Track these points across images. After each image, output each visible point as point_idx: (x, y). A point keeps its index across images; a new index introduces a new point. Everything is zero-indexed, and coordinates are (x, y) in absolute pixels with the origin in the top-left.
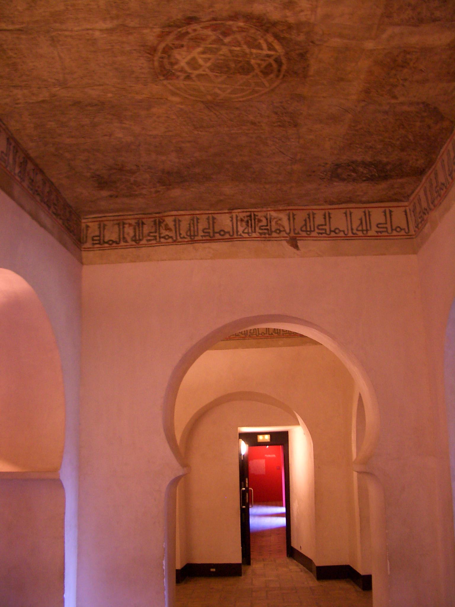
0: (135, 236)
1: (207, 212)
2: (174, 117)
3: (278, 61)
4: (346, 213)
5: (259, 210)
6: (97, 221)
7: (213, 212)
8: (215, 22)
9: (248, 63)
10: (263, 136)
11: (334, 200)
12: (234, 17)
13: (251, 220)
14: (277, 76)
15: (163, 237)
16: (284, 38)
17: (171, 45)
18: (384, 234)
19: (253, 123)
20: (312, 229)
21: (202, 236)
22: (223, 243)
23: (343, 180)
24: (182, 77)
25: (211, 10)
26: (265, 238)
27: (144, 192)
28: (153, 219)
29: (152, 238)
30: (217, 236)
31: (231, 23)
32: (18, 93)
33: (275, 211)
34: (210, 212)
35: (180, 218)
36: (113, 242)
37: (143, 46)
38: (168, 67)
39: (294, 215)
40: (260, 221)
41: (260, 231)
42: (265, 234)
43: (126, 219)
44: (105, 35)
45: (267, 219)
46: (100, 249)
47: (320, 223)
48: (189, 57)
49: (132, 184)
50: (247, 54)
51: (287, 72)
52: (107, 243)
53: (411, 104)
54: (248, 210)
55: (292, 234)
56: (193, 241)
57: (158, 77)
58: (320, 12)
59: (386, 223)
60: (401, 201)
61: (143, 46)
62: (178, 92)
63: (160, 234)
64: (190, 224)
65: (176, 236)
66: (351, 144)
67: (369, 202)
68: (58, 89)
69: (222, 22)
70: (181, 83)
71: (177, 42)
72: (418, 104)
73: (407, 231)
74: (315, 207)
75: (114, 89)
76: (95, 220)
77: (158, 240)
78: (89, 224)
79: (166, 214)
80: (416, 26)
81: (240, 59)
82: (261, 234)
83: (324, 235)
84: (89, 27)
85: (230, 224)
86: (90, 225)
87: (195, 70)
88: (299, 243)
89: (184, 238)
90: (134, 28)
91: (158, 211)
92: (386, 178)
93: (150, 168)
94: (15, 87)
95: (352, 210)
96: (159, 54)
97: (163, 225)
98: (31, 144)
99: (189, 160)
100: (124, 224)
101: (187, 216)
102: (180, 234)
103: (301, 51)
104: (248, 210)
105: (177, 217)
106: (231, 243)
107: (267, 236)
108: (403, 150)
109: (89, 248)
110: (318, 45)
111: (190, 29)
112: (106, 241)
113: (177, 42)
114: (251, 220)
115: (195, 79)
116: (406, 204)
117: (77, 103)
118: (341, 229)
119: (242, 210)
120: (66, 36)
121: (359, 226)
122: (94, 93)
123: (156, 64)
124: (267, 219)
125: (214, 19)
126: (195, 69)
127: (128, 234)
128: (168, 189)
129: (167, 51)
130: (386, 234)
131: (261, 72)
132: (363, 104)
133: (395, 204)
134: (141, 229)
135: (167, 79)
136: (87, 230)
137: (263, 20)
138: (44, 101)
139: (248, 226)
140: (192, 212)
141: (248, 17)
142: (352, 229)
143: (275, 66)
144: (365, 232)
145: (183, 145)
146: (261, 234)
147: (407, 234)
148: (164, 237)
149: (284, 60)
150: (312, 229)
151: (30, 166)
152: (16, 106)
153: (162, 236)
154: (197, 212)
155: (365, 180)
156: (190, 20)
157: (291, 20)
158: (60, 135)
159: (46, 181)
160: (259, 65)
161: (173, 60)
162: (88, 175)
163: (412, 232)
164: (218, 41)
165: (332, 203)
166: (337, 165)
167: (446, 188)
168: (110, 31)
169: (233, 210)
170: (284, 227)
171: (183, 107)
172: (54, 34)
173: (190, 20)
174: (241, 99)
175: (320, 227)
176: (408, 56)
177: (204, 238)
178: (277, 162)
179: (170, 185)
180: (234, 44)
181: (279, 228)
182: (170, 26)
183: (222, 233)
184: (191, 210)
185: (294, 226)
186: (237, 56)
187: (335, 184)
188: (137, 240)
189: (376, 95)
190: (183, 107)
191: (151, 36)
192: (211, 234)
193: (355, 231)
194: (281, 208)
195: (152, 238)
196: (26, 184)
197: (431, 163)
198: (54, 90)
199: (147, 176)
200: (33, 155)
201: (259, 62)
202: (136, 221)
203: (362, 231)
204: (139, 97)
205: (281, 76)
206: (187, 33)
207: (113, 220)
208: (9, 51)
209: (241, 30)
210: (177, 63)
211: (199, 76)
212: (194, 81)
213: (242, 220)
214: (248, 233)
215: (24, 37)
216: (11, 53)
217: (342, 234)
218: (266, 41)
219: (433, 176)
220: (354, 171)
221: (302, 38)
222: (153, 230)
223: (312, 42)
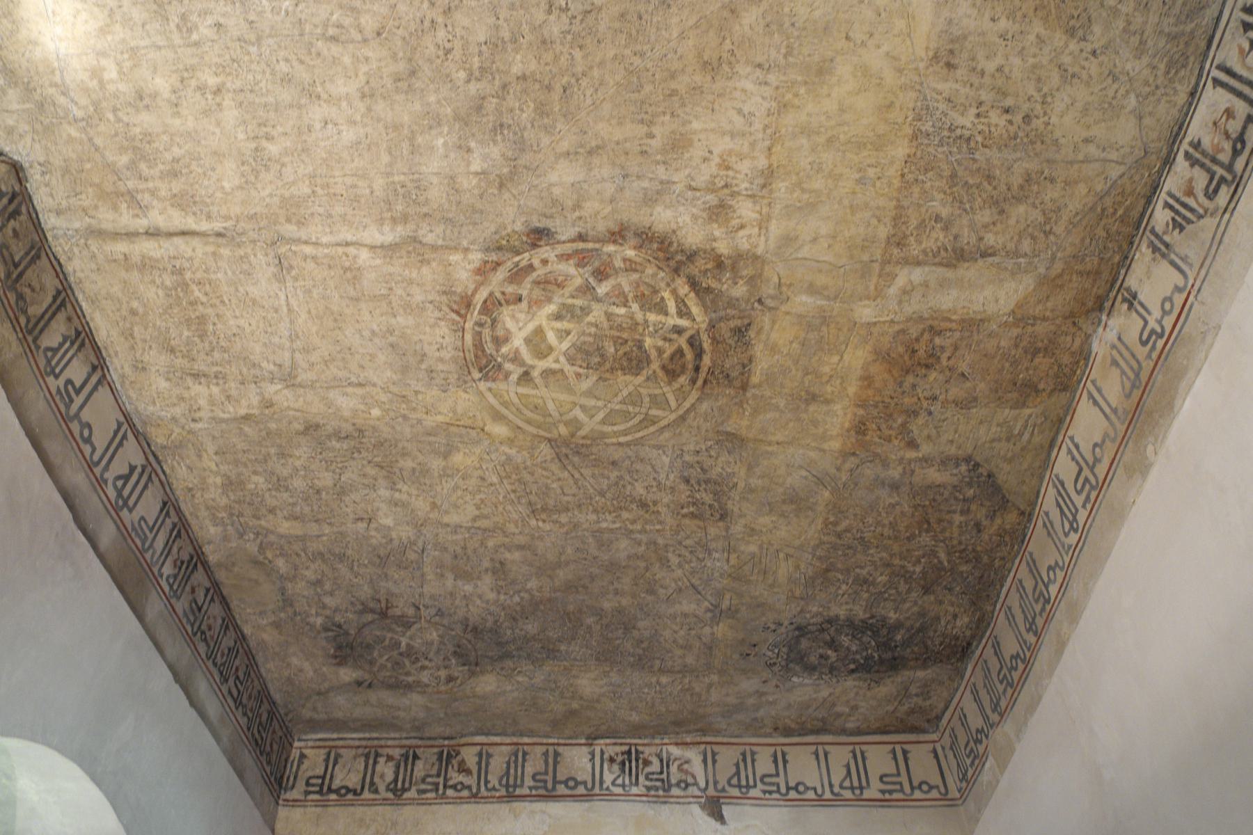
0: (396, 780)
1: (545, 741)
2: (495, 479)
3: (693, 342)
4: (816, 754)
5: (646, 741)
6: (325, 747)
7: (556, 741)
8: (581, 245)
9: (640, 345)
10: (661, 541)
11: (793, 726)
12: (618, 235)
13: (630, 762)
14: (693, 381)
15: (451, 787)
16: (708, 290)
17: (498, 295)
18: (895, 796)
19: (643, 505)
20: (751, 783)
21: (531, 788)
22: (572, 804)
23: (810, 669)
24: (514, 377)
25: (577, 214)
26: (658, 796)
27: (425, 677)
28: (436, 750)
29: (429, 787)
30: (561, 789)
31: (611, 248)
32: (200, 391)
33: (677, 744)
34: (551, 741)
35: (491, 750)
36: (348, 790)
37: (444, 293)
38: (490, 348)
39: (714, 754)
40: (647, 763)
41: (648, 783)
42: (657, 789)
43: (381, 747)
44: (378, 262)
45: (661, 761)
46: (317, 804)
47: (766, 772)
48: (531, 327)
49: (401, 654)
50: (637, 324)
51: (711, 372)
52: (337, 791)
53: (945, 462)
54: (623, 741)
55: (711, 792)
56: (511, 797)
57: (469, 373)
58: (775, 229)
59: (899, 774)
60: (924, 731)
61: (444, 293)
62: (504, 411)
63: (446, 780)
64: (508, 763)
65: (479, 784)
66: (827, 570)
67: (859, 732)
68: (279, 387)
69: (597, 246)
70: (511, 389)
71: (510, 289)
72: (957, 462)
73: (943, 790)
74: (753, 740)
75: (383, 397)
76: (321, 744)
77: (441, 792)
78: (306, 752)
79: (463, 740)
80: (948, 265)
81: (625, 335)
82: (648, 788)
83: (775, 796)
84: (349, 238)
85: (589, 766)
86: (309, 754)
87: (540, 359)
88: (726, 811)
89: (494, 789)
90: (434, 248)
91: (448, 732)
92: (894, 665)
93: (440, 613)
94: (196, 376)
95: (827, 748)
96: (475, 315)
97: (454, 762)
98: (212, 530)
99: (517, 599)
100: (377, 755)
101: (504, 748)
102: (487, 782)
103: (738, 323)
104: (623, 741)
105: (485, 747)
106: (587, 805)
107: (661, 793)
108: (927, 590)
109: (294, 801)
110: (770, 309)
111: (534, 257)
112: (334, 787)
113: (510, 289)
114: (629, 762)
115: (538, 381)
116: (934, 737)
117: (311, 428)
118: (809, 784)
119: (613, 741)
120: (305, 258)
121: (845, 779)
122: (346, 403)
123: (468, 337)
124: (661, 761)
125: (581, 238)
126: (541, 355)
127: (382, 776)
128: (472, 674)
129: (491, 307)
130: (900, 796)
131: (663, 367)
132: (851, 462)
133: (912, 737)
134: (409, 767)
135: (486, 377)
136: (300, 763)
137: (671, 244)
138: (246, 418)
139: (623, 771)
140: (515, 740)
141: (645, 237)
142: (831, 786)
143: (689, 355)
144: (858, 792)
145: (508, 555)
146: (648, 788)
147: (945, 796)
148: (454, 787)
149: (706, 345)
150: (751, 783)
151: (199, 577)
152: (193, 425)
153: (451, 783)
154: (526, 740)
155: (853, 671)
156: (539, 236)
157: (723, 248)
158: (272, 511)
159: (230, 623)
160: (660, 351)
161: (500, 333)
162: (319, 621)
163: (954, 793)
164: (587, 289)
165: (788, 732)
166: (799, 628)
167: (1023, 661)
168: (388, 250)
169: (595, 739)
170: (694, 777)
171: (513, 452)
172: (283, 249)
173: (539, 236)
174: (622, 439)
175: (767, 780)
176: (937, 341)
177: (534, 792)
178: (685, 615)
179: (477, 664)
180: (614, 299)
181: (684, 777)
182: (500, 248)
183: (571, 783)
184: (514, 735)
185: (714, 775)
186: (620, 328)
187: (795, 679)
188: (397, 791)
189: (877, 440)
190: (513, 452)
191: (463, 268)
192: (550, 785)
193: (836, 789)
194: (688, 740)
195: (429, 787)
196: (181, 605)
197: (982, 624)
198: (271, 389)
199: (434, 636)
200: (212, 558)
201: (660, 343)
202: (403, 751)
203: (852, 788)
204: (430, 421)
205: (700, 382)
206: (531, 267)
207: (358, 747)
208: (194, 287)
209: (631, 267)
210: (507, 340)
211: (547, 373)
212: (536, 387)
213: (612, 760)
214: (623, 786)
215: (225, 252)
216: (197, 293)
217: (811, 795)
218: (674, 292)
219: (989, 651)
220: (832, 644)
221: (740, 290)
222: (434, 772)
223: (760, 301)
